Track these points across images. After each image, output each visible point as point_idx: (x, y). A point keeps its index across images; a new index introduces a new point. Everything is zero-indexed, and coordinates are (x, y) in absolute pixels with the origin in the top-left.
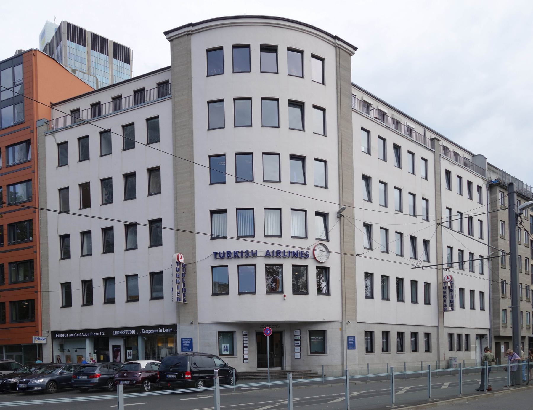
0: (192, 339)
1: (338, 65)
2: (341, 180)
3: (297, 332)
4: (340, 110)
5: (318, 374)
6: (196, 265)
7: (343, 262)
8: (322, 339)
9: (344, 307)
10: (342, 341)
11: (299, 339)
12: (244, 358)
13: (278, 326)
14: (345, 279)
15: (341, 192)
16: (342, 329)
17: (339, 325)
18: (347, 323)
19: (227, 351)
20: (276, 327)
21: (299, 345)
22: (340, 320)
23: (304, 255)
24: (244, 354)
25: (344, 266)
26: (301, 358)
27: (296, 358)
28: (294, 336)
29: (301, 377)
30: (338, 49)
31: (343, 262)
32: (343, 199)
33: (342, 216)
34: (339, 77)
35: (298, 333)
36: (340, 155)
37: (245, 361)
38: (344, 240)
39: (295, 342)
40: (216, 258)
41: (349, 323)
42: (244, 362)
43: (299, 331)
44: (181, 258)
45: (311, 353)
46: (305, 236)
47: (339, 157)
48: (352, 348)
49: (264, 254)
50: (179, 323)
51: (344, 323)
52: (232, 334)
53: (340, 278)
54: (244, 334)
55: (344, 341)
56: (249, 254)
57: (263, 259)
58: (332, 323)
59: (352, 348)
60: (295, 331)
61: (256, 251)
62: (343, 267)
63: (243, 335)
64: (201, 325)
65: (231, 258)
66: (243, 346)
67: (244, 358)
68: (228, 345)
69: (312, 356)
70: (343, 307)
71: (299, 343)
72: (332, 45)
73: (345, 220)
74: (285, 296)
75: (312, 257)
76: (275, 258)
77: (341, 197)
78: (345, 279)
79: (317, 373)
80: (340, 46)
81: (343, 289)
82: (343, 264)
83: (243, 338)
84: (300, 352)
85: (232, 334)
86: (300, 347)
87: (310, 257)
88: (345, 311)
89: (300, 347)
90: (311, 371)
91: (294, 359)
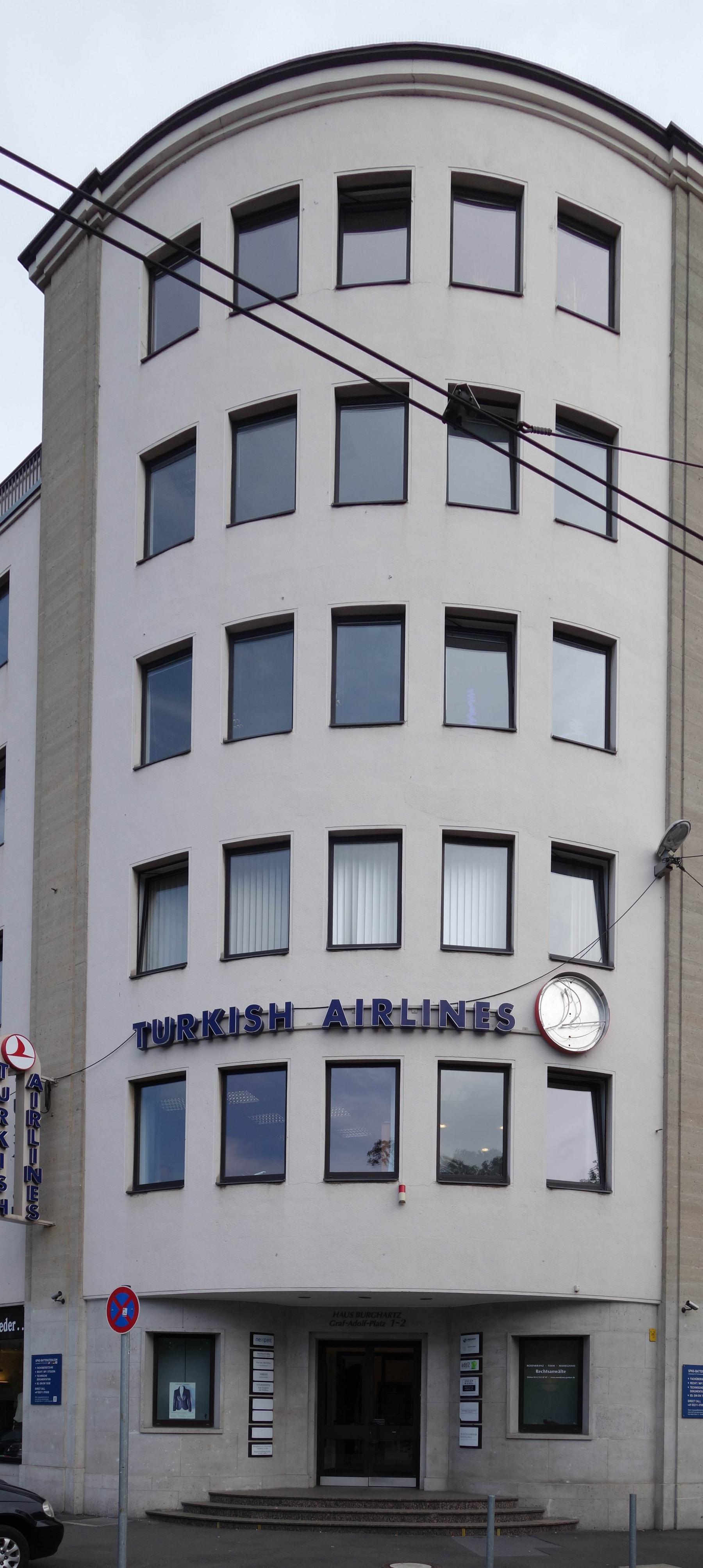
0: (59, 1357)
1: (682, 259)
2: (676, 724)
3: (468, 1343)
4: (682, 442)
5: (545, 1515)
6: (83, 1082)
7: (676, 1058)
8: (569, 1371)
9: (671, 1241)
10: (659, 1384)
11: (477, 1368)
12: (253, 1436)
13: (398, 1317)
14: (680, 1126)
15: (676, 773)
16: (658, 1336)
17: (647, 1319)
18: (684, 1310)
19: (187, 1407)
20: (393, 1321)
21: (476, 1393)
22: (654, 1295)
23: (492, 1023)
24: (253, 1424)
25: (680, 1075)
26: (480, 1446)
27: (462, 1443)
28: (83, 1304)
29: (460, 1528)
30: (680, 193)
31: (673, 1057)
32: (682, 802)
33: (674, 866)
34: (681, 306)
35: (472, 1346)
36: (677, 621)
37: (256, 1450)
38: (681, 968)
39: (463, 1381)
40: (143, 1047)
41: (693, 1308)
42: (253, 1454)
43: (477, 1337)
44: (20, 1052)
45: (524, 1427)
46: (503, 946)
47: (670, 631)
48: (46, 1399)
49: (318, 1018)
50: (29, 1299)
51: (671, 1308)
52: (208, 1341)
53: (658, 1125)
54: (255, 1343)
55: (667, 1382)
56: (258, 1021)
57: (316, 1037)
58: (614, 1307)
59: (46, 1399)
60: (463, 1338)
61: (288, 1005)
62: (673, 1078)
63: (253, 1348)
64: (92, 1305)
65: (196, 1041)
66: (251, 1392)
67: (253, 1436)
68: (192, 1386)
69: (525, 1442)
70: (668, 1242)
71: (473, 1388)
72: (658, 178)
73: (691, 888)
74: (401, 1189)
75: (532, 1029)
76: (366, 1035)
77: (676, 792)
78: (680, 1126)
79: (542, 1512)
80: (690, 182)
81: (672, 1170)
82: (673, 1068)
83: (252, 1358)
84: (477, 1425)
85: (208, 1341)
86: (477, 1404)
87: (517, 1027)
88: (675, 1262)
89: (477, 1404)
90: (516, 1500)
91: (456, 1449)
